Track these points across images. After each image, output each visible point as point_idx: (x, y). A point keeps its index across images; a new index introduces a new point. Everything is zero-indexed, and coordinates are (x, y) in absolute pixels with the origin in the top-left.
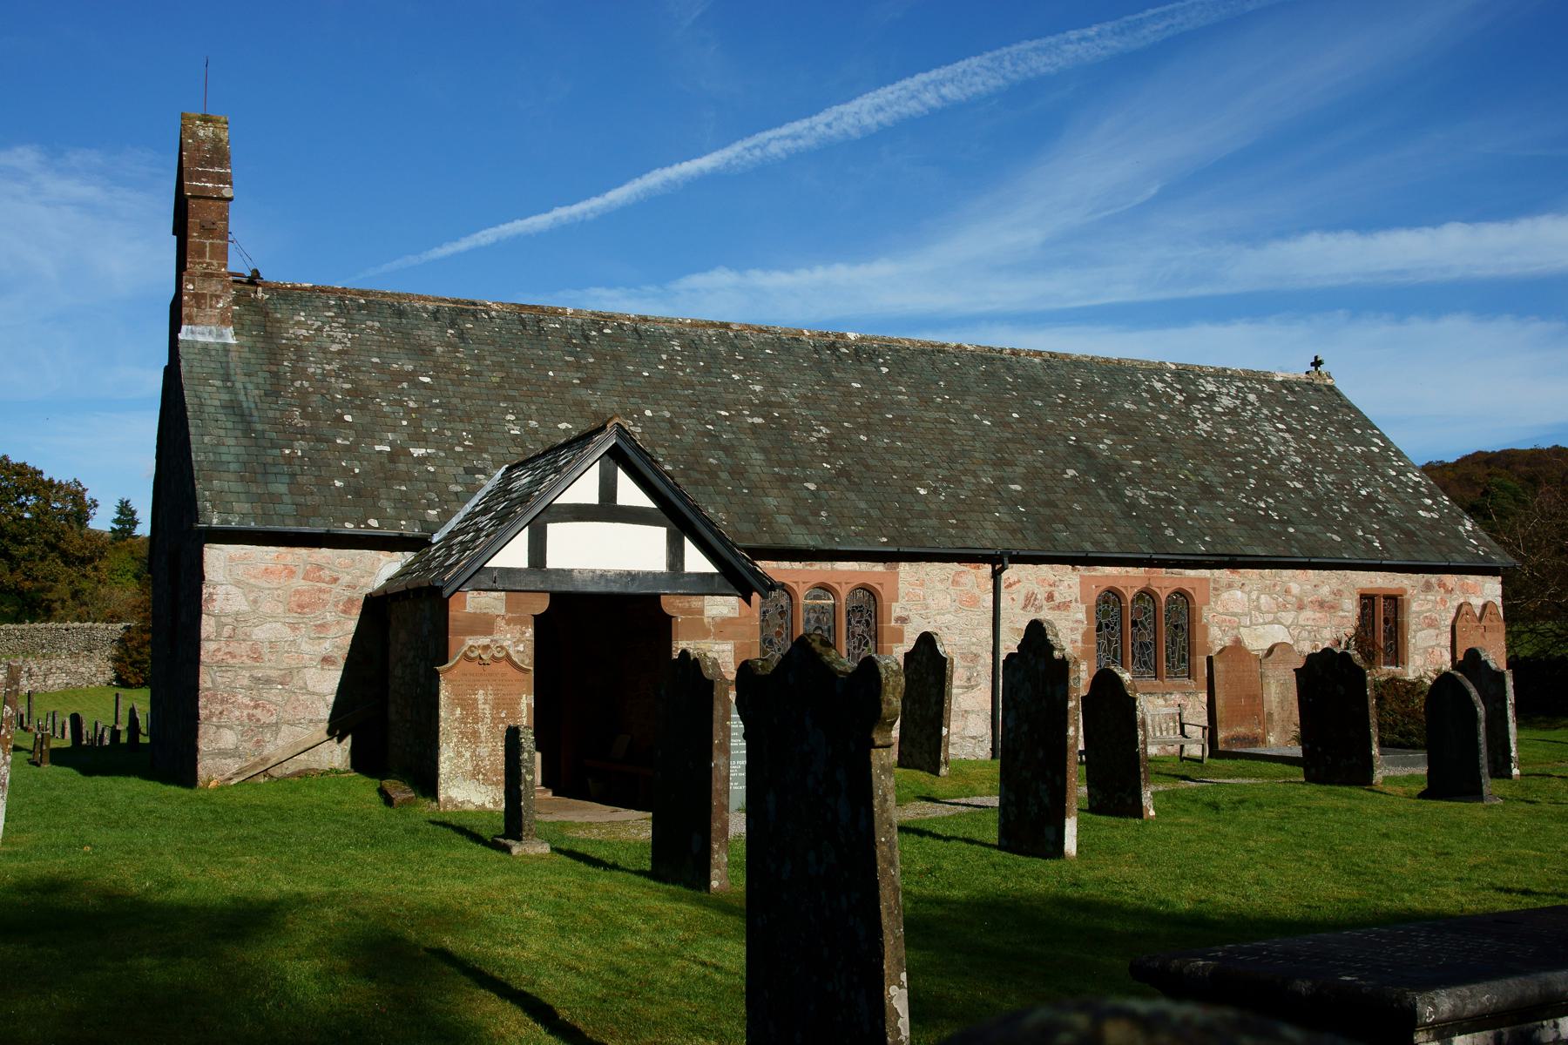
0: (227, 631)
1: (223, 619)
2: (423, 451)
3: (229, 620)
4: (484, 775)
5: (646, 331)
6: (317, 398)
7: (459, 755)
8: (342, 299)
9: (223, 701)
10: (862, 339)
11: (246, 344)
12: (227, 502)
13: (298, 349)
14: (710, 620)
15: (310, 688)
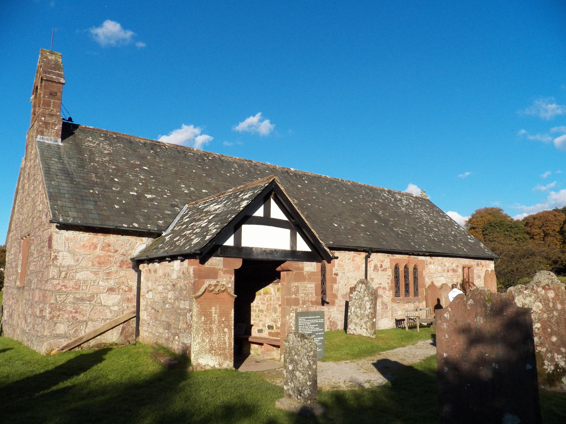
0: (63, 274)
2: (150, 196)
4: (215, 350)
5: (224, 160)
6: (101, 170)
7: (203, 341)
8: (106, 134)
9: (59, 310)
10: (296, 171)
11: (67, 146)
12: (66, 211)
13: (90, 151)
14: (306, 273)
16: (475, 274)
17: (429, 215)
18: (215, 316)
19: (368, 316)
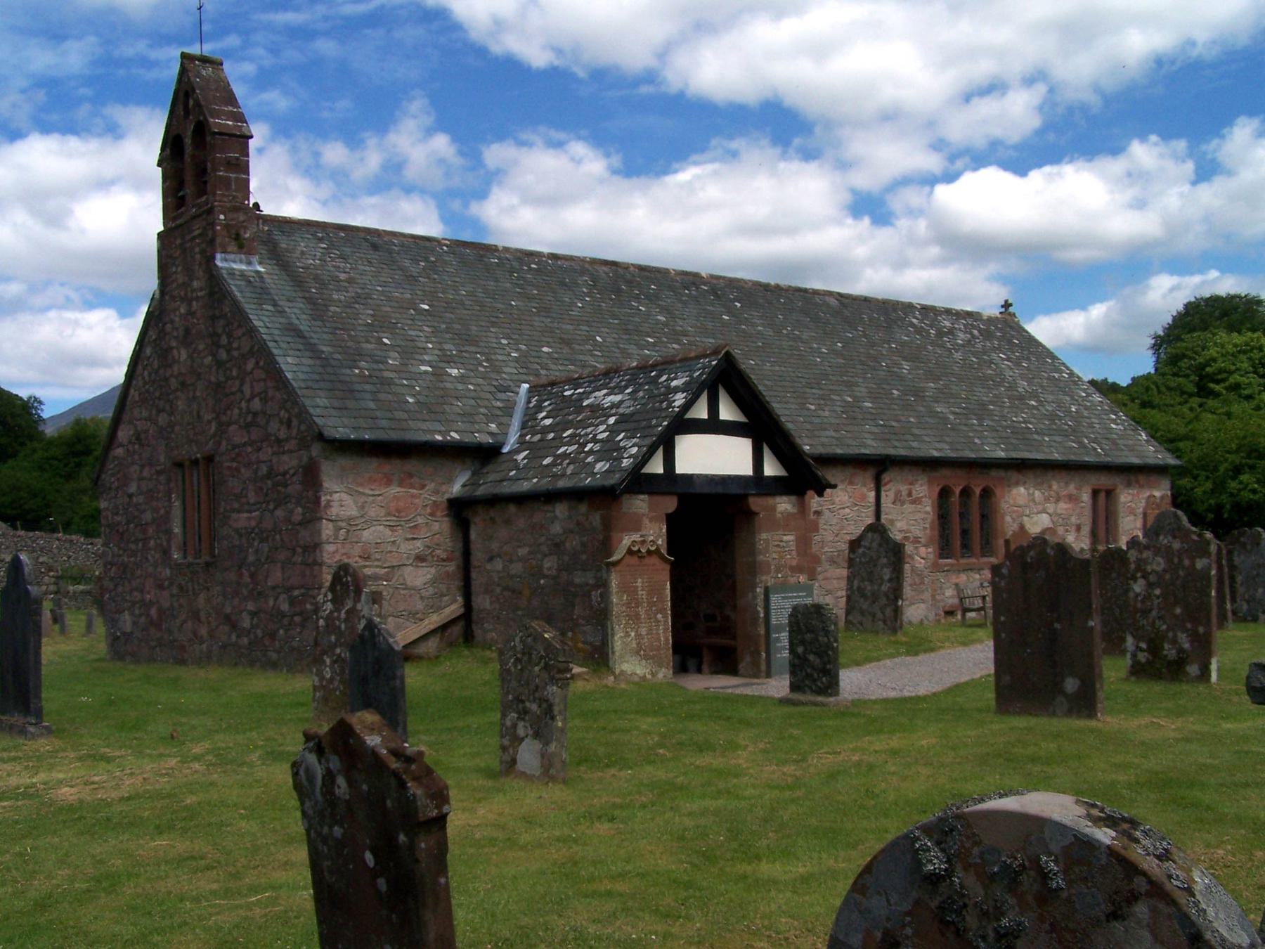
1: (340, 523)
3: (344, 524)
7: (628, 635)
15: (409, 583)
16: (1121, 506)
17: (1018, 364)
18: (642, 594)
19: (886, 594)
